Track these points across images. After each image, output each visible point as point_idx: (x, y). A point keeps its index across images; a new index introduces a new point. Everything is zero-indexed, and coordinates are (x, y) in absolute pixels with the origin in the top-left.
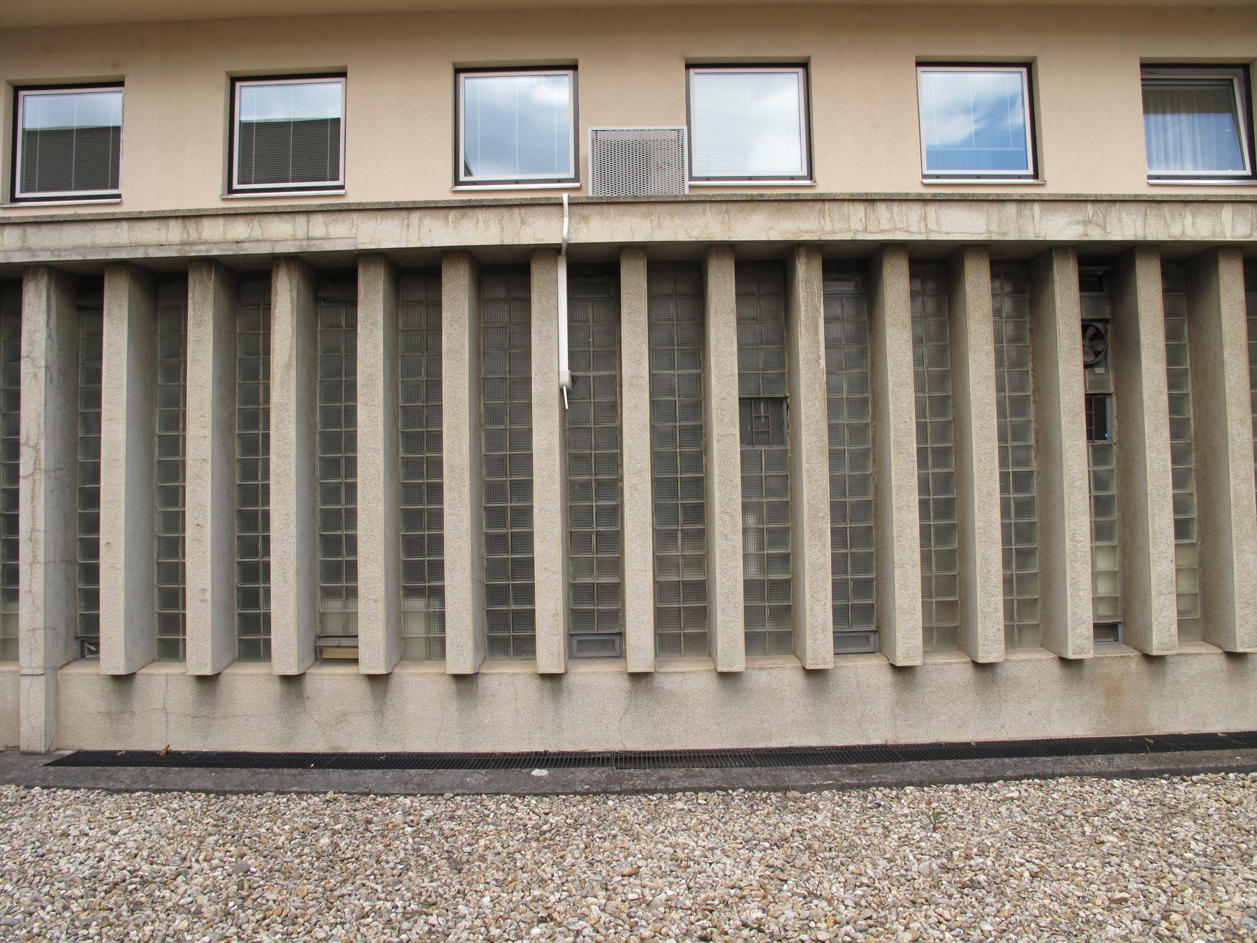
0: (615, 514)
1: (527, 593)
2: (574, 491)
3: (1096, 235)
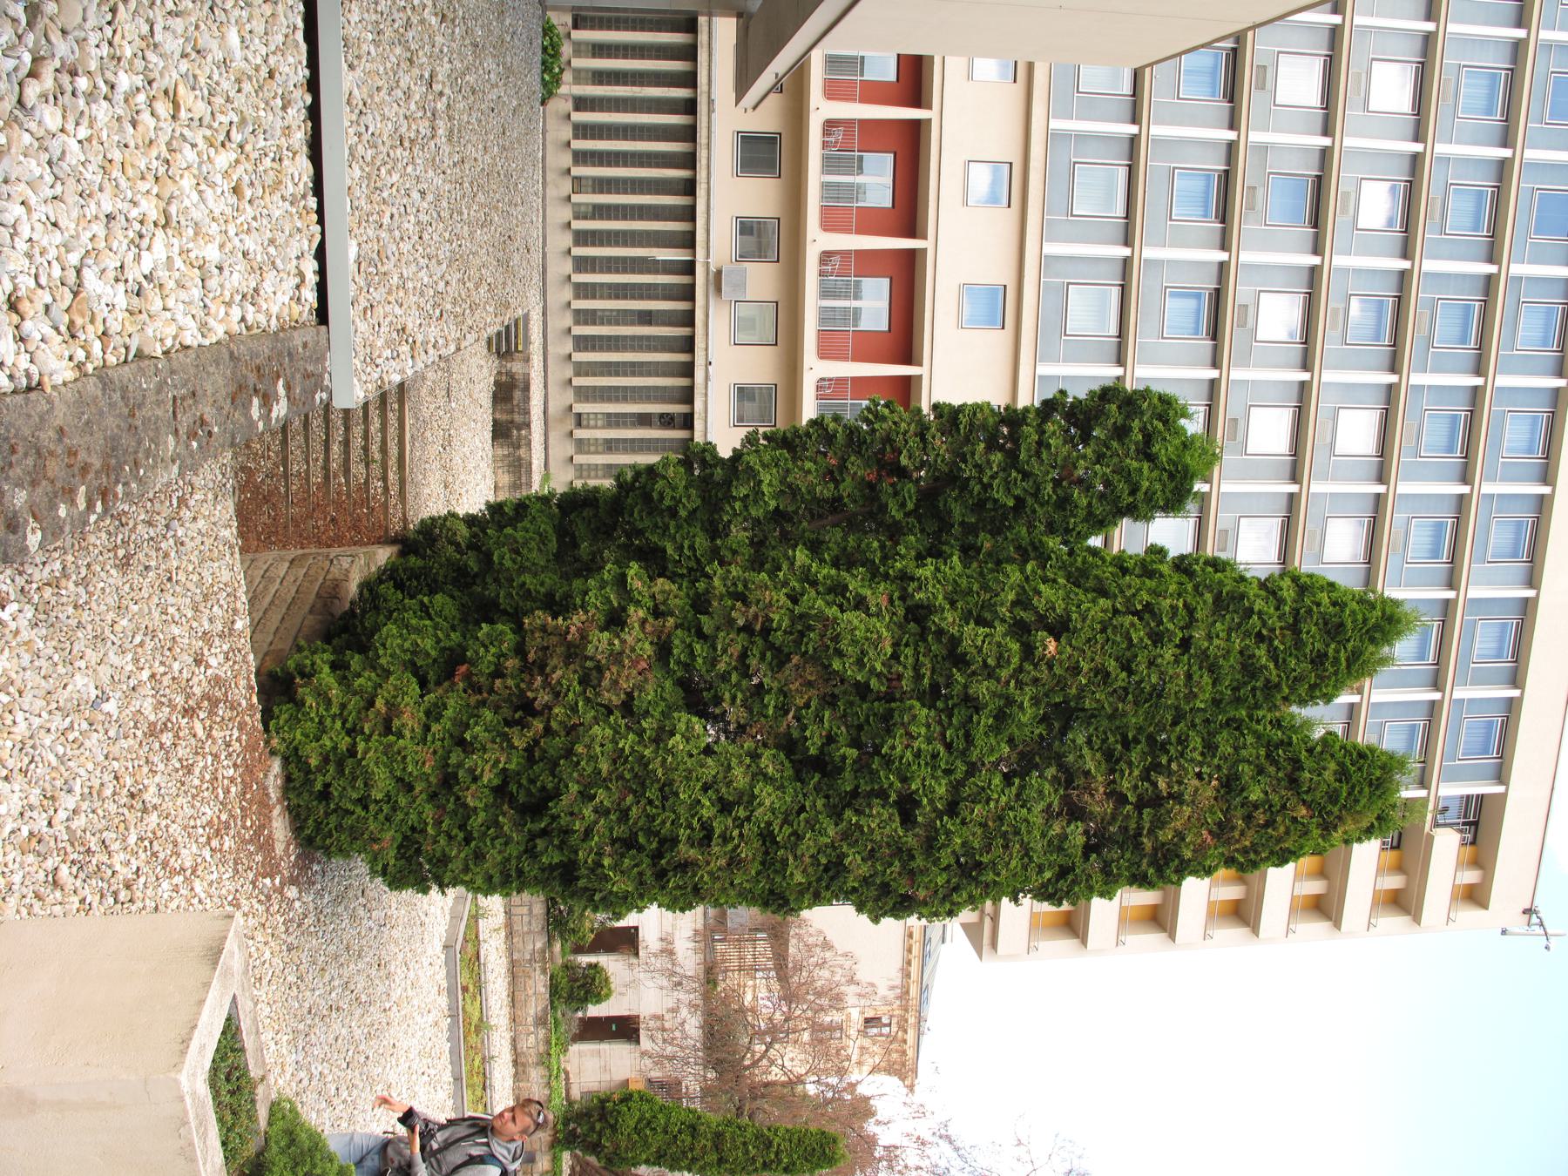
0: (617, 271)
1: (593, 245)
3: (696, 416)
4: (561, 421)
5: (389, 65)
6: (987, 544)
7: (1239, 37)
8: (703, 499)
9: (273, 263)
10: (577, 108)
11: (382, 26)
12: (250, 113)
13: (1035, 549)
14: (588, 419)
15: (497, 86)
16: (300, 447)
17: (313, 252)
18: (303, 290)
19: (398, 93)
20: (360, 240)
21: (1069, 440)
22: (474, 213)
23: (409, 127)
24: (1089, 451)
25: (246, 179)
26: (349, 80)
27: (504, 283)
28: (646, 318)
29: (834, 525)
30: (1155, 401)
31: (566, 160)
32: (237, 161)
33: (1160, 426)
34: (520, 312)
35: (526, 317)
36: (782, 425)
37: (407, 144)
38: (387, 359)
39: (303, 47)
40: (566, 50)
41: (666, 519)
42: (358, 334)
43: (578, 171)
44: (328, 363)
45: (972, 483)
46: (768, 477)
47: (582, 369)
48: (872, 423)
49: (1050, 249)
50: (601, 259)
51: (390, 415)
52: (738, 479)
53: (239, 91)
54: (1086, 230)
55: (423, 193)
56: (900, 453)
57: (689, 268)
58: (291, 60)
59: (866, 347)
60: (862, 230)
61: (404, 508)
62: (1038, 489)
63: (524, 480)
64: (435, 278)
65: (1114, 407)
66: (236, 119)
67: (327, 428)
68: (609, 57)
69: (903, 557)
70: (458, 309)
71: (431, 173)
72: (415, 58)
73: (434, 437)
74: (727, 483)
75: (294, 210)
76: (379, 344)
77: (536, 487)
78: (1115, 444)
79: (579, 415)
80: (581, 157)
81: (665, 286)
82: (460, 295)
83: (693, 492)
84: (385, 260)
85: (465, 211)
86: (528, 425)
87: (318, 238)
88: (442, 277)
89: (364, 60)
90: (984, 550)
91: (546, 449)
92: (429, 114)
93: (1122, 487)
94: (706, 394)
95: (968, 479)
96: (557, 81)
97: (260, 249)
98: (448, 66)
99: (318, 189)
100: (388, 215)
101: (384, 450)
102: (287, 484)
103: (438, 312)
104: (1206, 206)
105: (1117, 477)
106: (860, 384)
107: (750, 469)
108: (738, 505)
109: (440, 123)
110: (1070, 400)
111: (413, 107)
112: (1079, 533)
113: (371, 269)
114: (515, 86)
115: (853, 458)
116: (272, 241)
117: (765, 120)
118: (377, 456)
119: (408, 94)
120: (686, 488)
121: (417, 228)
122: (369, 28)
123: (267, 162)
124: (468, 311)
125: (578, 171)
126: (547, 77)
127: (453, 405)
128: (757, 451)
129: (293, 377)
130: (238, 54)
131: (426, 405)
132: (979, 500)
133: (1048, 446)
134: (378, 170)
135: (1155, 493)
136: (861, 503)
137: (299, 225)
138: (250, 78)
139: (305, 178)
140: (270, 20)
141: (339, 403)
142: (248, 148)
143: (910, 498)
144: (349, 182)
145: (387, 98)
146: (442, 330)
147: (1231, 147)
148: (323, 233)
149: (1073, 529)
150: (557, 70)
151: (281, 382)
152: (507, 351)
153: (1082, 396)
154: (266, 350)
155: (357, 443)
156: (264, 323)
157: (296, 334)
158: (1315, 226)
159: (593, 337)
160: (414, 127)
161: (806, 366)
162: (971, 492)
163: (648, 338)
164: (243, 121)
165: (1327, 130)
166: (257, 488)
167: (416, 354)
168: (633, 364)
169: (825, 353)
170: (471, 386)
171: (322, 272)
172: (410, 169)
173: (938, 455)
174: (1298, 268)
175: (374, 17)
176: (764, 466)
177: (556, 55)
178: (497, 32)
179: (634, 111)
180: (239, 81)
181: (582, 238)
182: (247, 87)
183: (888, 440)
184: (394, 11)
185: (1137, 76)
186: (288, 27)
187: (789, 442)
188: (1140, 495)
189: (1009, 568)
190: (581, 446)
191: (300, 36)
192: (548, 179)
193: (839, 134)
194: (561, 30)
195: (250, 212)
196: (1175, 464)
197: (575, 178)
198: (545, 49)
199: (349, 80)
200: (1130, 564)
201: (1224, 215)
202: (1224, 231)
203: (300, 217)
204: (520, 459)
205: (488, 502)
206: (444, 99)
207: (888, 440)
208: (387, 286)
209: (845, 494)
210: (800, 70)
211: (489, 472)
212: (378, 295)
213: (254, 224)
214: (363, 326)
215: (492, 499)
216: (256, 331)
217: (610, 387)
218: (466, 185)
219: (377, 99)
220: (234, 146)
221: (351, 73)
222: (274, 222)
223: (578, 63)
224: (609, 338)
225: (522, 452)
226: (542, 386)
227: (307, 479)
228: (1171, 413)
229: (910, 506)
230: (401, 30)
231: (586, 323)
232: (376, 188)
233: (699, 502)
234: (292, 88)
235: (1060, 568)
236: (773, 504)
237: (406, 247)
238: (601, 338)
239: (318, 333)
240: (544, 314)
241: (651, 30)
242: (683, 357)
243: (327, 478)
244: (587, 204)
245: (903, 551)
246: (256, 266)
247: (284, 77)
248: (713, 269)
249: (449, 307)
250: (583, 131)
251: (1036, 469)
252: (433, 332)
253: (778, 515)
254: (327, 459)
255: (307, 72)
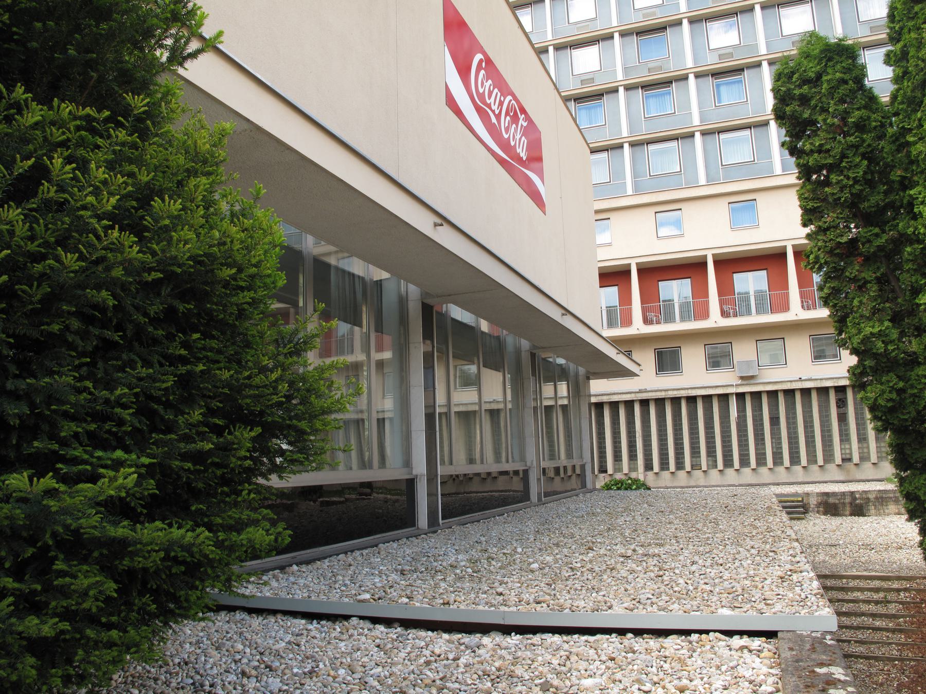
0: (747, 440)
1: (732, 456)
2: (739, 436)
3: (836, 385)
4: (848, 471)
5: (613, 583)
6: (898, 173)
7: (566, 99)
8: (889, 371)
9: (732, 668)
10: (651, 469)
11: (590, 587)
12: (634, 675)
13: (897, 139)
14: (845, 454)
15: (634, 516)
16: (879, 648)
17: (727, 638)
18: (752, 648)
19: (630, 577)
20: (719, 606)
21: (815, 133)
22: (708, 530)
23: (651, 571)
24: (820, 118)
25: (676, 682)
26: (618, 609)
27: (755, 510)
28: (775, 421)
29: (898, 279)
30: (779, 83)
31: (682, 474)
32: (664, 688)
33: (796, 76)
34: (774, 500)
35: (777, 495)
36: (832, 330)
37: (661, 573)
38: (802, 590)
39: (599, 636)
40: (619, 476)
41: (907, 395)
42: (783, 610)
43: (688, 467)
44: (804, 633)
45: (854, 191)
46: (867, 329)
47: (812, 459)
48: (821, 264)
49: (702, 180)
50: (740, 450)
51: (851, 585)
52: (872, 349)
53: (620, 681)
54: (688, 162)
55: (693, 563)
56: (839, 243)
57: (741, 396)
58: (605, 645)
59: (779, 282)
60: (706, 294)
61: (919, 578)
62: (852, 146)
63: (892, 495)
64: (748, 555)
65: (788, 109)
66: (637, 686)
67: (864, 628)
68: (621, 452)
69: (916, 228)
70: (770, 540)
71: (681, 558)
72: (611, 566)
73: (865, 556)
74: (875, 356)
75: (699, 650)
76: (791, 595)
77: (891, 487)
78: (813, 103)
79: (843, 460)
80: (680, 465)
81: (753, 411)
82: (761, 539)
83: (884, 379)
84: (734, 589)
85: (707, 535)
86: (852, 493)
87: (717, 634)
88: (748, 550)
89: (607, 599)
90: (903, 174)
91: (869, 481)
92: (645, 558)
93: (842, 90)
94: (821, 379)
95: (852, 194)
96: (636, 481)
97: (722, 677)
98: (618, 546)
99: (687, 633)
100: (704, 587)
101: (877, 590)
102: (908, 660)
103: (771, 554)
104: (663, 95)
105: (836, 95)
106: (803, 282)
107: (863, 342)
108: (890, 347)
109: (651, 551)
110: (788, 139)
111: (640, 568)
112: (883, 117)
113: (740, 599)
114: (635, 505)
115: (847, 274)
116: (718, 668)
117: (647, 359)
118: (881, 595)
119: (632, 571)
120: (882, 384)
121: (715, 567)
122: (589, 595)
123: (666, 666)
124: (771, 534)
125: (688, 467)
126: (634, 487)
127: (841, 542)
128: (850, 338)
129: (814, 660)
130: (597, 680)
131: (840, 561)
132: (866, 184)
133: (821, 145)
134: (675, 592)
135: (844, 67)
136: (879, 264)
137: (708, 647)
138: (613, 673)
139: (679, 641)
140: (580, 657)
141: (835, 628)
142: (656, 679)
143: (871, 231)
144: (681, 612)
145: (632, 585)
146: (784, 551)
147: (628, 88)
148: (715, 631)
149: (880, 122)
150: (630, 481)
151: (818, 670)
152: (803, 507)
153: (783, 131)
154: (794, 679)
155: (872, 608)
156: (775, 679)
157: (783, 655)
158: (665, 28)
159: (790, 453)
160: (652, 568)
161: (795, 318)
162: (861, 191)
163: (787, 418)
164: (639, 681)
165: (610, 37)
166: (913, 681)
167: (799, 569)
168: (805, 427)
169: (785, 307)
170: (828, 531)
171: (741, 633)
172: (677, 571)
173: (837, 218)
174: (692, 31)
175: (584, 591)
176: (860, 332)
177: (621, 482)
178: (604, 517)
179: (650, 436)
180: (614, 681)
181: (728, 463)
182: (618, 676)
183: (831, 252)
184: (582, 579)
185: (593, 151)
186: (586, 646)
187: (841, 320)
188: (847, 77)
189: (914, 153)
190: (864, 458)
191: (591, 639)
192: (694, 484)
193: (651, 315)
194: (608, 479)
195: (697, 682)
196: (821, 60)
197: (692, 468)
198: (619, 489)
199: (618, 609)
200: (900, 71)
201: (667, 83)
202: (676, 80)
203: (704, 646)
204: (876, 498)
205: (907, 520)
206: (637, 549)
207: (831, 252)
208: (751, 588)
209: (874, 275)
210: (615, 342)
211: (888, 519)
212: (757, 595)
213: (705, 679)
214: (778, 607)
215: (906, 516)
216: (780, 686)
217: (822, 441)
218: (691, 535)
219: (632, 592)
220: (653, 689)
221: (614, 607)
222: (705, 665)
223: (626, 469)
224: (790, 443)
225: (871, 496)
226: (825, 485)
227: (903, 645)
228: (786, 71)
229: (877, 230)
230: (594, 574)
231: (782, 458)
232: (687, 594)
233: (891, 374)
234: (622, 646)
235: (909, 119)
236: (887, 323)
237: (726, 575)
238: (790, 448)
239: (783, 639)
240: (778, 484)
241: (604, 429)
242: (798, 396)
243: (901, 631)
244: (707, 461)
245: (912, 229)
246: (734, 681)
247: (615, 650)
248: (740, 382)
249: (768, 546)
250: (664, 465)
251: (837, 151)
252: (784, 557)
253: (896, 319)
254: (887, 630)
255: (614, 635)
